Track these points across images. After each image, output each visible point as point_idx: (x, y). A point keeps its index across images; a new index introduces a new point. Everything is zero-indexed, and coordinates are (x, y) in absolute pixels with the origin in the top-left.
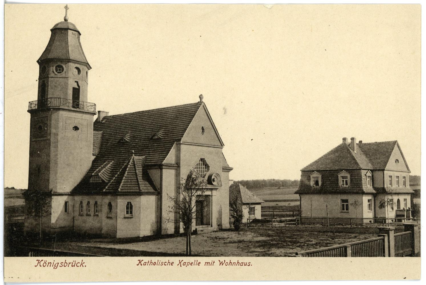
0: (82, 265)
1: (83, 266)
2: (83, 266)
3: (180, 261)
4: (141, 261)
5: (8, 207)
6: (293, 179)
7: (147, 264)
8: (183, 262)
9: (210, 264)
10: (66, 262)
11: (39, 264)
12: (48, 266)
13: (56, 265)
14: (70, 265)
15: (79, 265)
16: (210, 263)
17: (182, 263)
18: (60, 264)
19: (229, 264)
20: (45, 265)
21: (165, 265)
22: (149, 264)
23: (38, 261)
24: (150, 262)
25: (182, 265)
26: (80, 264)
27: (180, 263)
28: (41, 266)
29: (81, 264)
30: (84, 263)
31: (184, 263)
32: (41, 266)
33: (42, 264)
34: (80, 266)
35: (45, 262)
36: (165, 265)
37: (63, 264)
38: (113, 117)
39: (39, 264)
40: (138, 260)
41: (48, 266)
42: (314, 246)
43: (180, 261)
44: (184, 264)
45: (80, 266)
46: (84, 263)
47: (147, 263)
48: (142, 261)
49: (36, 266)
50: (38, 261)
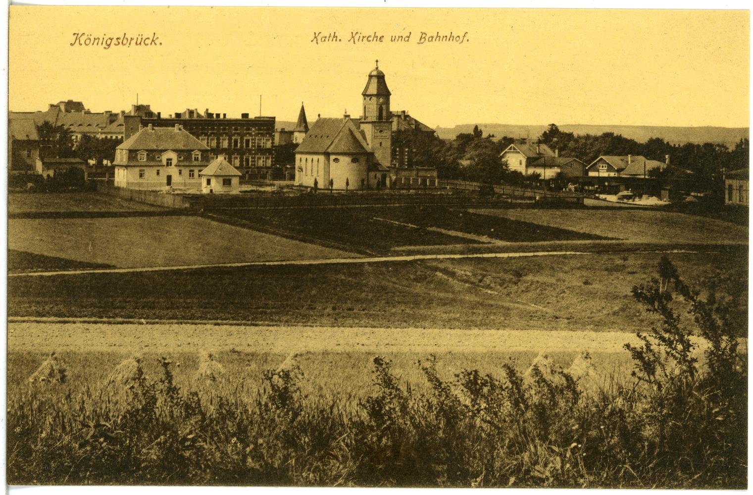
0: (153, 43)
1: (155, 44)
2: (155, 44)
3: (315, 33)
4: (79, 35)
5: (20, 254)
6: (293, 121)
7: (327, 39)
8: (321, 35)
9: (100, 43)
10: (376, 35)
11: (78, 41)
12: (93, 44)
13: (109, 42)
14: (134, 42)
15: (148, 42)
16: (101, 40)
17: (357, 37)
18: (114, 41)
19: (92, 42)
20: (88, 42)
21: (146, 45)
22: (331, 39)
23: (76, 35)
24: (332, 35)
25: (319, 41)
26: (372, 38)
27: (353, 37)
28: (81, 44)
29: (153, 41)
30: (158, 38)
31: (110, 38)
32: (81, 44)
33: (82, 42)
34: (151, 44)
35: (89, 37)
36: (146, 45)
37: (120, 41)
38: (624, 138)
39: (78, 41)
40: (74, 34)
41: (93, 44)
42: (266, 458)
43: (315, 33)
44: (323, 39)
45: (151, 44)
46: (158, 38)
47: (328, 38)
48: (83, 37)
49: (72, 44)
50: (76, 35)
